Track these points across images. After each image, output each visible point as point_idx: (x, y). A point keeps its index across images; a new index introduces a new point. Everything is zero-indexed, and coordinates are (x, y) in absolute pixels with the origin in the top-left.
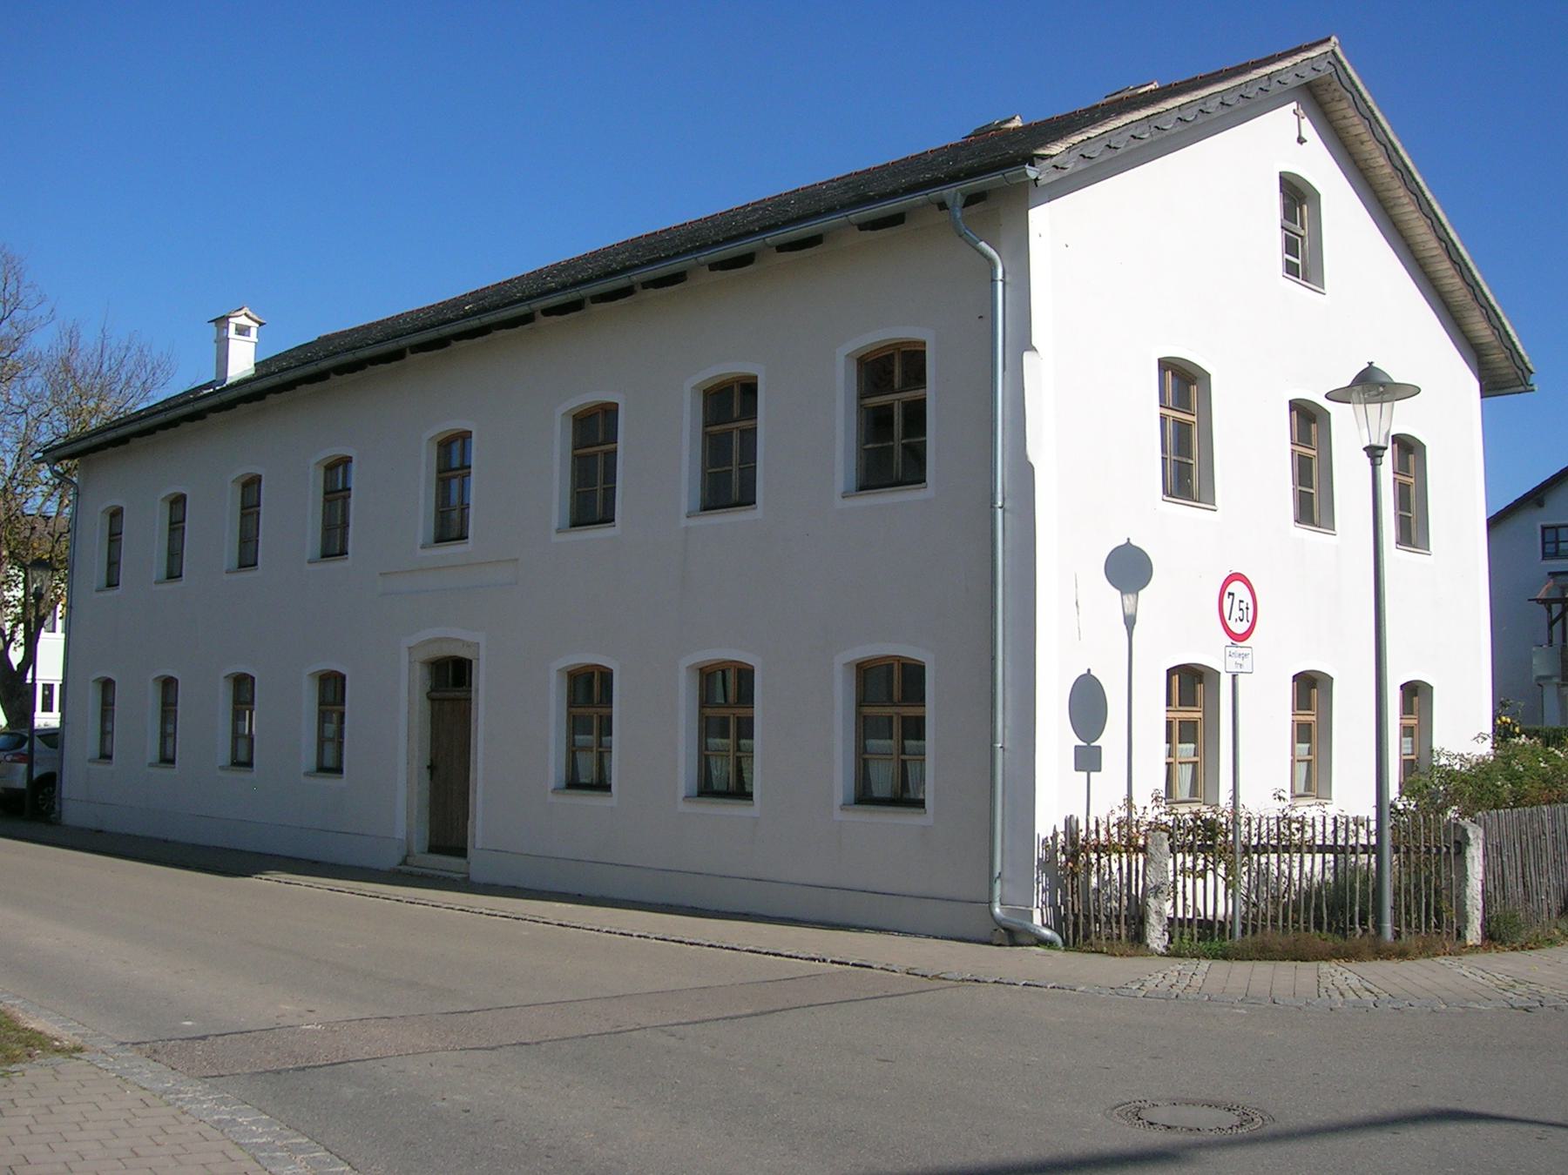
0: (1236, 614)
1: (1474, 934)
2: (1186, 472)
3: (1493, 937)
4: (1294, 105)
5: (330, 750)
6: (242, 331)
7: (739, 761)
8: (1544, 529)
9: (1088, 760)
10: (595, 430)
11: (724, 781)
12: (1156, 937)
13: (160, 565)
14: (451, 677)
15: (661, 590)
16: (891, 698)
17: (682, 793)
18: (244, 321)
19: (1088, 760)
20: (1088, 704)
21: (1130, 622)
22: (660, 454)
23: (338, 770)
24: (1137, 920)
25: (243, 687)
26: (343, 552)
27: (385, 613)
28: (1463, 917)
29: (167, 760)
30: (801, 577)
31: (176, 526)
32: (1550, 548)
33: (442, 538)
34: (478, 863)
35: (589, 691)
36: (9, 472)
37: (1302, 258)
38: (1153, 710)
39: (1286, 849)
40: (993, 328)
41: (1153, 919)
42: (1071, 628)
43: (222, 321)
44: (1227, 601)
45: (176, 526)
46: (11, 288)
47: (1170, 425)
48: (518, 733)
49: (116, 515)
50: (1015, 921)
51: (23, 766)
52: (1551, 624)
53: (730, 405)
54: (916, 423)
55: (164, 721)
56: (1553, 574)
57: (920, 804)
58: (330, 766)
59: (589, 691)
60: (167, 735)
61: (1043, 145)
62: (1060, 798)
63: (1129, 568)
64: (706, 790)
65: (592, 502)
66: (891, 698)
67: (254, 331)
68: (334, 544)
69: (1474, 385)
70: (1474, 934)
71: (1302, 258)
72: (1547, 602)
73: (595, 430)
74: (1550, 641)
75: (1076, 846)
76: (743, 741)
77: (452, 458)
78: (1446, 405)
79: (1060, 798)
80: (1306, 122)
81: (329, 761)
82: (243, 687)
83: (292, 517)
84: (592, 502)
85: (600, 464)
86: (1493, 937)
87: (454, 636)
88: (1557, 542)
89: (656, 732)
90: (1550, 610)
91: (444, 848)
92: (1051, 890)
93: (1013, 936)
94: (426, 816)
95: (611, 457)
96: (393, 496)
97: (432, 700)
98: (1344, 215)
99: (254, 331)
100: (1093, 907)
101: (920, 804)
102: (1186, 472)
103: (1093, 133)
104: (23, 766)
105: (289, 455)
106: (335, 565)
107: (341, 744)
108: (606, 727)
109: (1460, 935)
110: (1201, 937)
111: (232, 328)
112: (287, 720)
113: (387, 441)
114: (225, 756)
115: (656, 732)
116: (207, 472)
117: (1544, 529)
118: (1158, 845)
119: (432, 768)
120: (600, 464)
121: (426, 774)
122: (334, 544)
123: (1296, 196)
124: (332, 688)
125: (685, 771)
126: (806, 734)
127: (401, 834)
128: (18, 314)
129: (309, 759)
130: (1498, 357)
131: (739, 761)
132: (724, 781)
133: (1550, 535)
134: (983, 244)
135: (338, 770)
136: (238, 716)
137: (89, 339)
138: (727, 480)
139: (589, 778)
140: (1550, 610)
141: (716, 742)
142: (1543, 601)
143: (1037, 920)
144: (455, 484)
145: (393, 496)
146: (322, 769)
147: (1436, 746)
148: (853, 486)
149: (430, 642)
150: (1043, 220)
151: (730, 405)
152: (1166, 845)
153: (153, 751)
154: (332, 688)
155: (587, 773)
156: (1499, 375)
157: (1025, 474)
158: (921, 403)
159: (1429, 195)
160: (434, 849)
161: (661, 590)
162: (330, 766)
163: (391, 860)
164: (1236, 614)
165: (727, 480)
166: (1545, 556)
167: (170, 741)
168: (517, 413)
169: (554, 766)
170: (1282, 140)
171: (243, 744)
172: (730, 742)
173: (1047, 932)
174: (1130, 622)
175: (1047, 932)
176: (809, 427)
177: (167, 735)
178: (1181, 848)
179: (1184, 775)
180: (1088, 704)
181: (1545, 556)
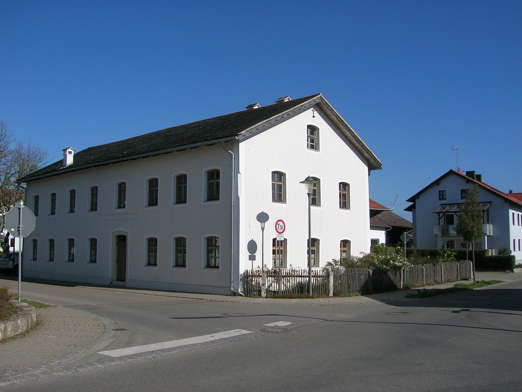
0: (280, 228)
1: (331, 294)
2: (279, 195)
3: (335, 295)
4: (312, 109)
5: (93, 257)
6: (70, 153)
7: (184, 259)
8: (439, 191)
9: (252, 258)
10: (153, 184)
11: (180, 263)
12: (263, 294)
13: (49, 211)
14: (122, 240)
15: (167, 221)
16: (211, 244)
17: (172, 266)
18: (70, 150)
19: (252, 258)
20: (252, 246)
21: (263, 229)
22: (167, 191)
23: (95, 262)
24: (260, 291)
25: (71, 242)
26: (96, 210)
27: (106, 225)
28: (329, 291)
29: (51, 260)
30: (192, 219)
31: (53, 200)
32: (441, 197)
33: (119, 207)
34: (128, 282)
35: (152, 243)
36: (2, 181)
37: (313, 143)
38: (269, 248)
39: (291, 276)
40: (232, 167)
41: (263, 290)
42: (248, 229)
43: (65, 150)
44: (277, 226)
45: (53, 200)
46: (4, 131)
47: (276, 185)
48: (136, 252)
49: (37, 197)
50: (235, 291)
51: (11, 262)
52: (440, 219)
53: (181, 180)
54: (219, 187)
55: (50, 250)
56: (441, 205)
57: (218, 267)
58: (93, 261)
59: (152, 243)
60: (35, 253)
61: (240, 132)
62: (245, 265)
63: (263, 218)
64: (177, 265)
65: (153, 201)
66: (211, 244)
67: (73, 153)
68: (94, 207)
69: (366, 168)
70: (331, 294)
71: (313, 143)
72: (438, 213)
73: (153, 184)
74: (439, 224)
75: (246, 275)
76: (210, 254)
77: (122, 188)
78: (357, 173)
79: (245, 265)
80: (316, 113)
81: (93, 260)
82: (71, 242)
83: (83, 200)
84: (153, 201)
85: (155, 191)
86: (335, 295)
87: (123, 230)
88: (443, 195)
89: (166, 252)
90: (439, 215)
91: (120, 279)
92: (243, 285)
93: (235, 294)
94: (116, 273)
95: (157, 190)
96: (108, 196)
97: (117, 245)
98: (327, 134)
99: (73, 153)
100: (250, 286)
101: (218, 267)
102: (279, 195)
103: (253, 127)
104: (11, 262)
105: (82, 185)
106: (94, 213)
107: (96, 256)
108: (156, 251)
109: (328, 294)
110: (275, 295)
111: (68, 152)
112: (82, 250)
113: (107, 181)
114: (67, 258)
115: (166, 252)
116: (61, 188)
117: (439, 191)
118: (264, 275)
119: (118, 261)
120: (155, 191)
121: (116, 263)
122: (94, 207)
123: (312, 130)
124: (94, 242)
125: (172, 261)
126: (196, 252)
127: (110, 277)
128: (6, 139)
129: (88, 259)
130: (372, 161)
131: (184, 259)
132: (180, 263)
133: (441, 194)
134: (230, 151)
135: (95, 262)
136: (70, 249)
137: (25, 146)
138: (181, 198)
139: (152, 262)
140: (439, 215)
141: (179, 255)
142: (437, 213)
143: (240, 290)
144: (123, 194)
145: (108, 196)
146: (91, 262)
147: (351, 255)
148: (206, 199)
149: (117, 232)
150: (242, 145)
151: (181, 180)
152: (266, 276)
153: (48, 258)
154: (94, 242)
155: (152, 262)
156: (372, 165)
157: (238, 199)
158: (219, 182)
159: (349, 126)
160: (118, 280)
161: (167, 221)
162: (93, 261)
163: (108, 282)
164: (280, 228)
165: (181, 198)
166: (440, 199)
167: (52, 256)
168: (136, 177)
169: (145, 260)
170: (310, 117)
171: (71, 256)
172: (182, 254)
173: (241, 293)
174: (263, 229)
175: (241, 293)
176: (197, 187)
177: (35, 253)
178: (269, 276)
179: (312, 261)
180: (252, 246)
181: (440, 199)
